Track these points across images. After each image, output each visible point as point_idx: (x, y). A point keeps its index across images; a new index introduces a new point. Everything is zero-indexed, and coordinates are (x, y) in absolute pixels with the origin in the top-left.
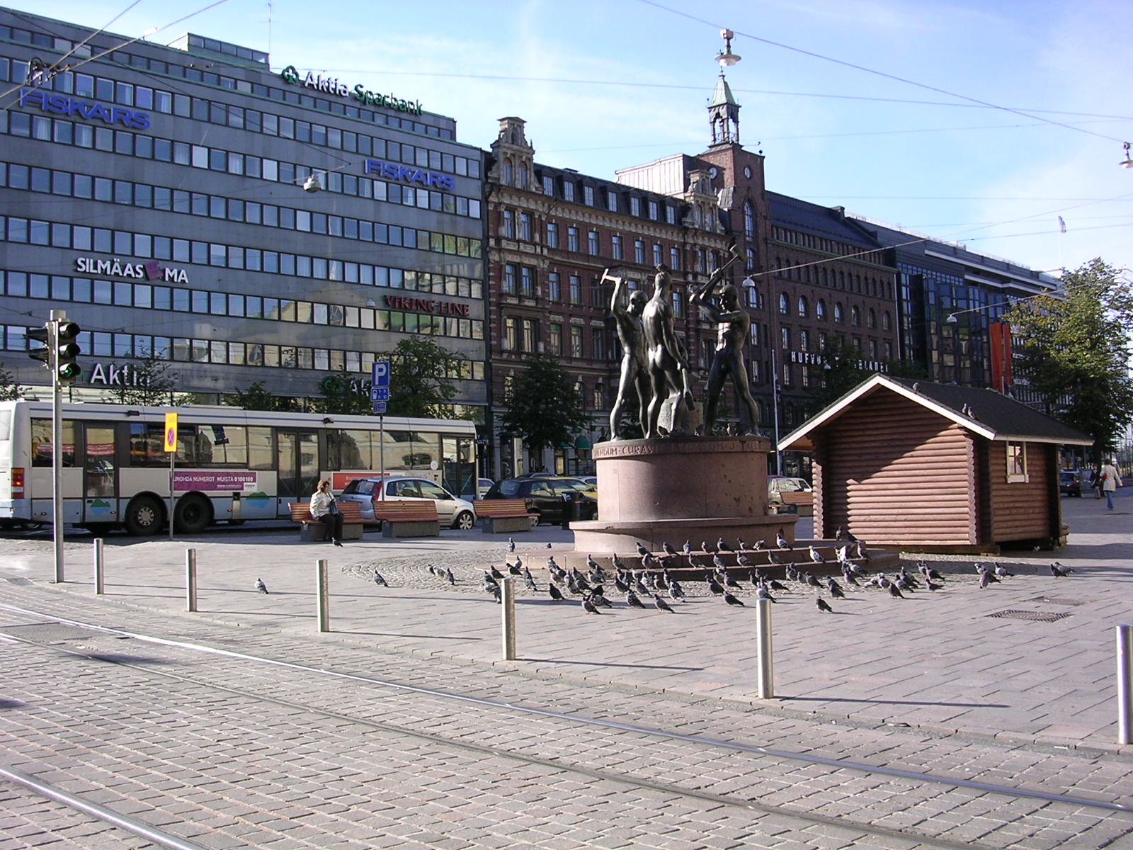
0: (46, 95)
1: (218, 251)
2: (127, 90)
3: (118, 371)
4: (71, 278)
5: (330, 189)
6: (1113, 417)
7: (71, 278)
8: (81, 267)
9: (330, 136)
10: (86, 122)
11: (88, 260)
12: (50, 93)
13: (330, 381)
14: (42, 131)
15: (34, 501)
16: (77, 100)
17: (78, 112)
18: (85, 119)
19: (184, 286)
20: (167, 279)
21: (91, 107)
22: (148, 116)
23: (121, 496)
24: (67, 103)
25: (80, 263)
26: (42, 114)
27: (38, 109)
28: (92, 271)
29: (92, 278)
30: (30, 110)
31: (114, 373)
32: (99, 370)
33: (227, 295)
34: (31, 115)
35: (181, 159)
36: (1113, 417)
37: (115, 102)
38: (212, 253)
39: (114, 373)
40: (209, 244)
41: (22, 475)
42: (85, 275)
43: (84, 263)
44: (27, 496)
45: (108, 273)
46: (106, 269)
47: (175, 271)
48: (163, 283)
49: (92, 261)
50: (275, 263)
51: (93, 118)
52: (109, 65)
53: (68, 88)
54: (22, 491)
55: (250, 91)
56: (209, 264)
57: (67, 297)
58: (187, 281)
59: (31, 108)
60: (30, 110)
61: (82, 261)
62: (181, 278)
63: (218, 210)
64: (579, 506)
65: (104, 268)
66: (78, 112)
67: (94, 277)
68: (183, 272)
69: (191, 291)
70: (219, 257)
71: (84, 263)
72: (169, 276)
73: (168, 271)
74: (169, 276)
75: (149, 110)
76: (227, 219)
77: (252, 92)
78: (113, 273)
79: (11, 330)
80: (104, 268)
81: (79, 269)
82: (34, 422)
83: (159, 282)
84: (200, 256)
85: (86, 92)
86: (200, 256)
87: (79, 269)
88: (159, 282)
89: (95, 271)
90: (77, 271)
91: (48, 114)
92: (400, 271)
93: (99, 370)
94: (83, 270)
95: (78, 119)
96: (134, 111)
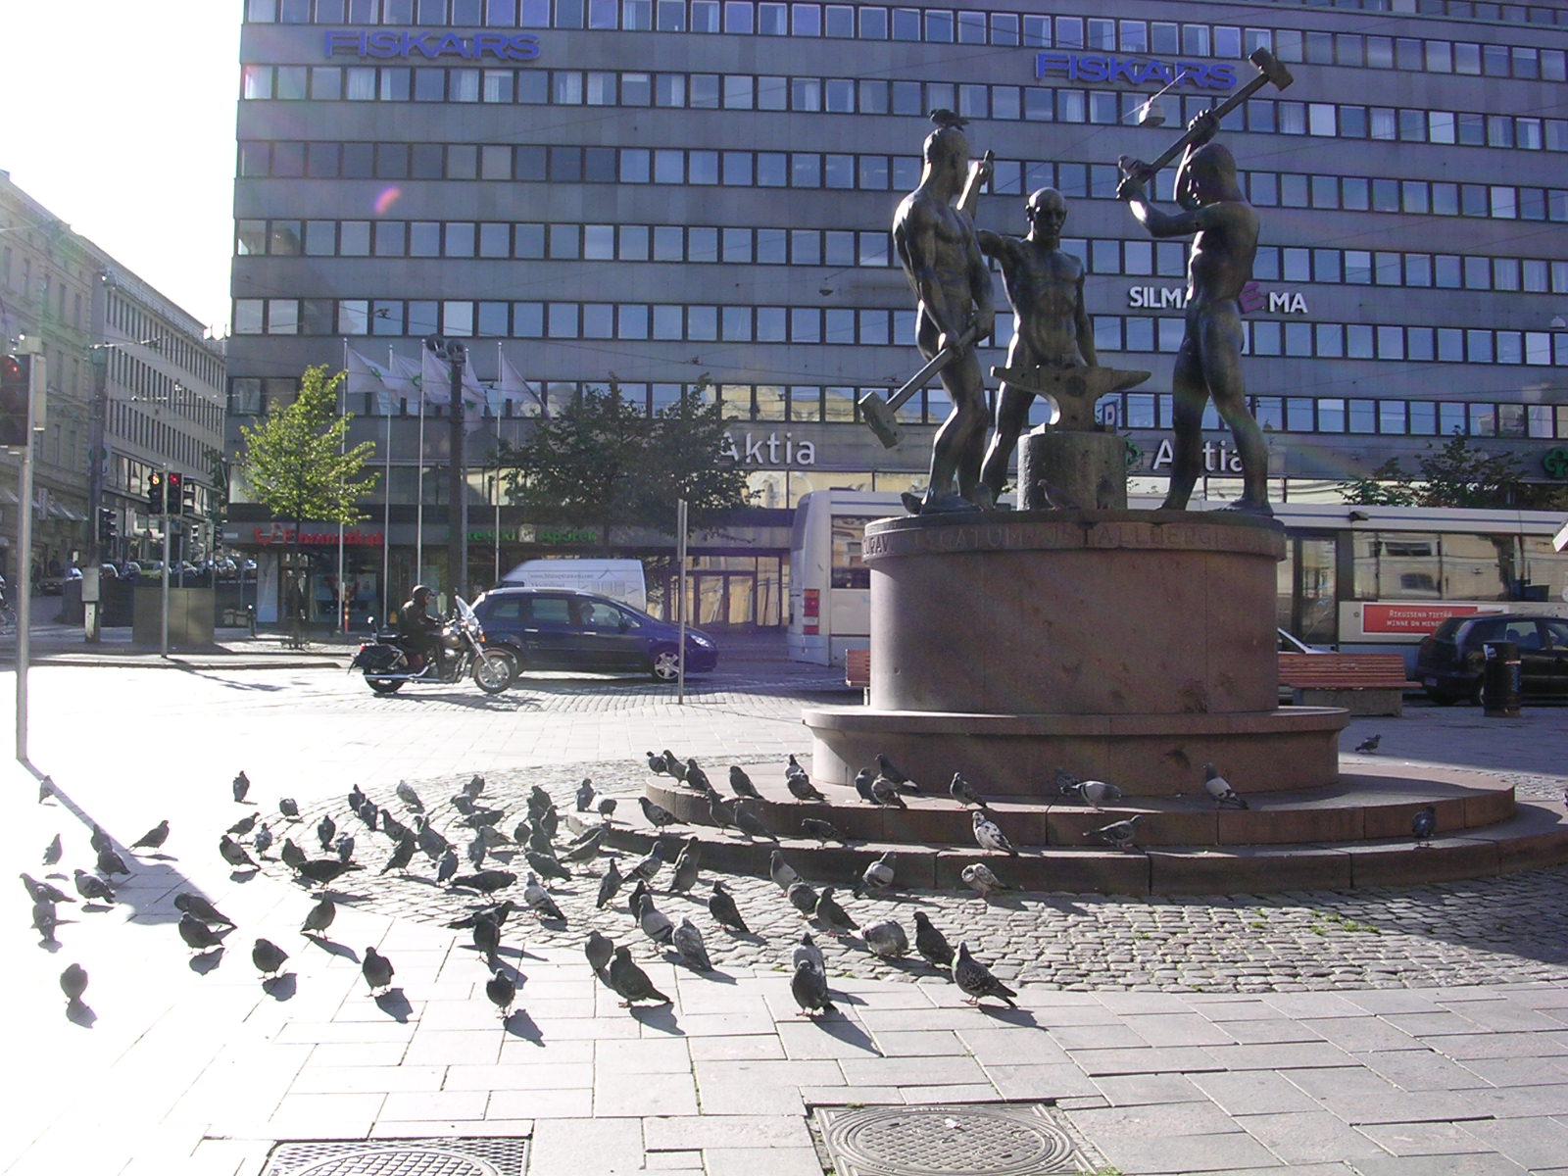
0: (1073, 58)
1: (1357, 261)
2: (779, 12)
3: (760, 443)
4: (1123, 318)
5: (1549, 147)
6: (601, 438)
7: (1123, 318)
8: (1136, 301)
9: (1545, 63)
10: (1138, 89)
11: (1146, 289)
12: (1079, 55)
13: (1553, 456)
14: (1073, 110)
15: (834, 638)
16: (1122, 59)
17: (1123, 76)
18: (1135, 85)
19: (1302, 318)
20: (1272, 309)
21: (1144, 66)
22: (535, 38)
23: (1341, 640)
24: (1107, 65)
25: (1132, 293)
26: (1069, 85)
27: (1064, 80)
28: (1152, 305)
29: (1155, 315)
30: (1052, 82)
31: (753, 446)
32: (1166, 449)
33: (1375, 327)
34: (1055, 90)
35: (1292, 126)
36: (601, 438)
37: (1181, 54)
38: (1347, 265)
39: (753, 446)
40: (1342, 252)
41: (817, 600)
42: (1144, 312)
43: (1141, 294)
44: (824, 630)
45: (1287, 310)
46: (1175, 300)
47: (1286, 297)
48: (1265, 316)
49: (1152, 290)
50: (1456, 272)
51: (1146, 81)
52: (1299, 10)
53: (1109, 44)
54: (815, 623)
55: (1414, 11)
56: (1343, 282)
57: (1118, 345)
58: (1305, 311)
59: (1052, 79)
60: (1052, 82)
61: (1137, 292)
62: (1295, 305)
63: (1356, 197)
64: (1515, 670)
65: (1171, 299)
66: (1123, 76)
67: (1158, 313)
68: (1298, 296)
69: (1314, 324)
70: (1362, 270)
71: (1141, 294)
72: (1276, 304)
73: (1273, 296)
74: (1276, 304)
75: (1235, 59)
76: (1371, 210)
77: (1418, 11)
78: (1293, 310)
79: (1322, 404)
80: (1280, 304)
81: (1132, 304)
82: (839, 522)
83: (1262, 315)
84: (1327, 268)
85: (1138, 46)
86: (1327, 268)
87: (1132, 304)
88: (1258, 315)
89: (1159, 305)
90: (1129, 306)
91: (370, 61)
92: (1543, 264)
93: (1166, 449)
94: (1139, 304)
95: (1125, 86)
96: (1210, 64)
